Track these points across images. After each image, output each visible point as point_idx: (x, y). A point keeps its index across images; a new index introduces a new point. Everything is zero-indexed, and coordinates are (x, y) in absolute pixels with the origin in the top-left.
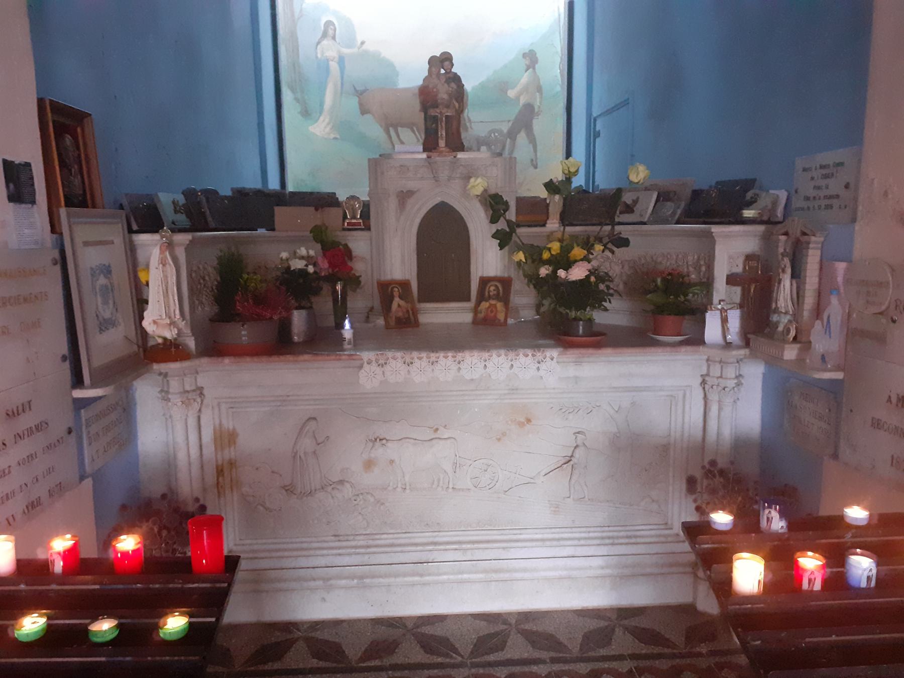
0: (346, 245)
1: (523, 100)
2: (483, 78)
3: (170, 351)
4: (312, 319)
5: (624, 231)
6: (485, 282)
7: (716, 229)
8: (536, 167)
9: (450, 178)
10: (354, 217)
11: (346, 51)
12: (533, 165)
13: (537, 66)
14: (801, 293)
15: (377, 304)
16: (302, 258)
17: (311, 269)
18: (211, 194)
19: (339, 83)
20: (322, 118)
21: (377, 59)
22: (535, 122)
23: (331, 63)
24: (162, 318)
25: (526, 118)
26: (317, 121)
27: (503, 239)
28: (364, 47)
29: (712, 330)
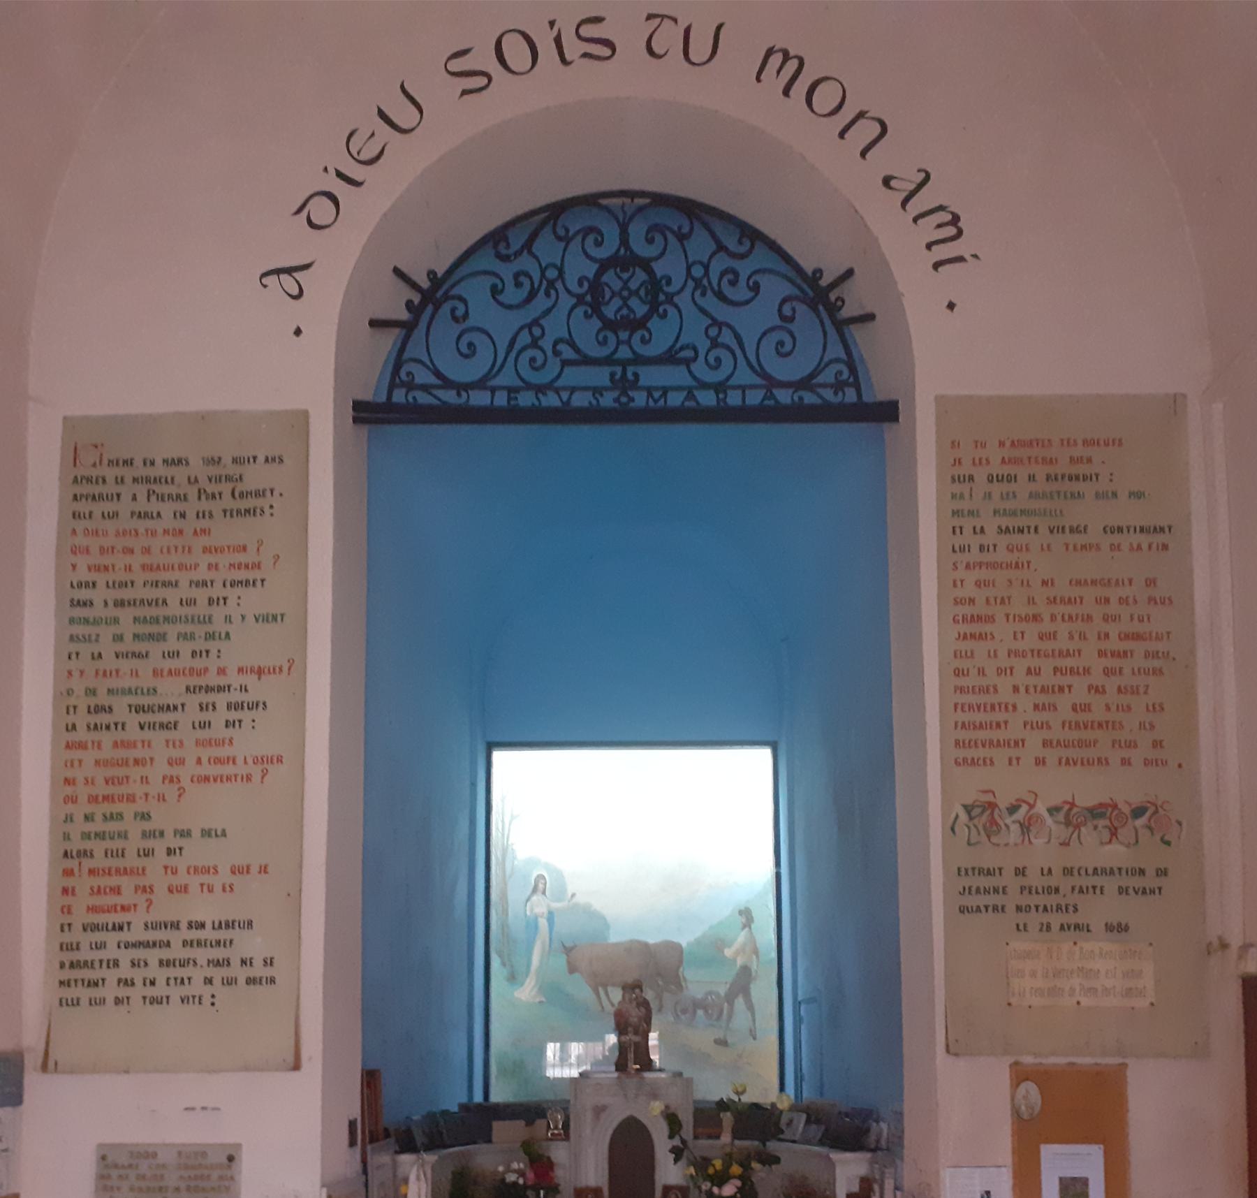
0: (549, 1158)
1: (740, 962)
2: (698, 934)
7: (836, 1156)
8: (755, 1038)
9: (637, 1096)
10: (556, 1128)
16: (515, 1171)
17: (521, 1181)
18: (445, 1113)
22: (752, 986)
25: (743, 982)
26: (522, 985)
27: (678, 1153)
28: (574, 900)
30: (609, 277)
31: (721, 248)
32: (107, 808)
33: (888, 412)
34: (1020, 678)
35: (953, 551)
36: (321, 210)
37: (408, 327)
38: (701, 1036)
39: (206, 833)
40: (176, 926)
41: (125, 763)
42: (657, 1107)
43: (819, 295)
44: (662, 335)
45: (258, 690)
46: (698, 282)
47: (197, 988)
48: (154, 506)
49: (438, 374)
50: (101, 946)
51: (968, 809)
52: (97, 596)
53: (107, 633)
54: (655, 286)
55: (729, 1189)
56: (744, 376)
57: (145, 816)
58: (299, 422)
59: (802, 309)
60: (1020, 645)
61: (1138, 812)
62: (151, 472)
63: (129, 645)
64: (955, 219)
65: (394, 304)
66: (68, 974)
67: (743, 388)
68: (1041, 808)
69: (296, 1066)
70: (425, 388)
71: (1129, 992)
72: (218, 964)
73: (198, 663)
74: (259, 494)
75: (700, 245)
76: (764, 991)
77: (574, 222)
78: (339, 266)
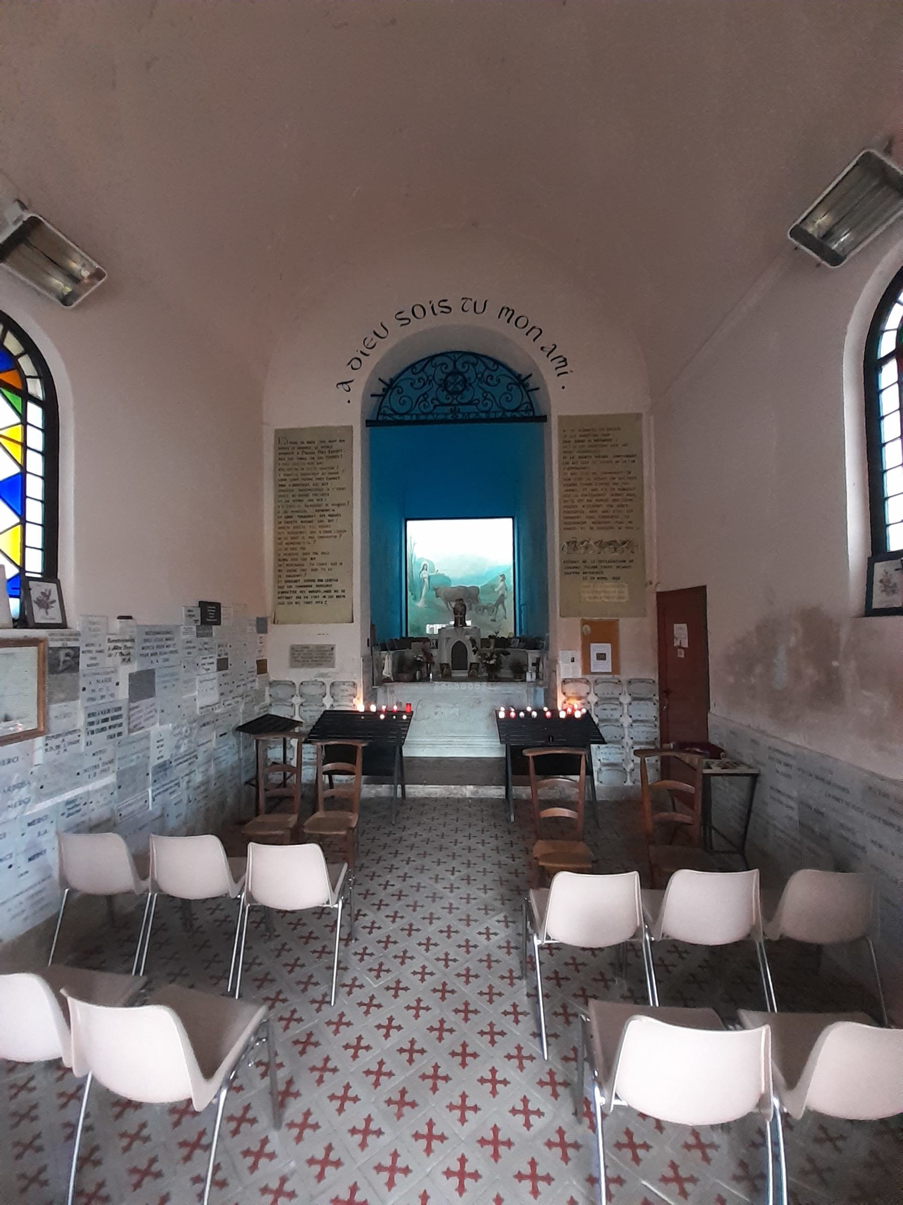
1: (501, 593)
3: (388, 680)
4: (421, 674)
5: (508, 650)
6: (471, 664)
7: (528, 651)
14: (157, 629)
15: (439, 670)
24: (387, 672)
25: (501, 600)
27: (475, 652)
29: (528, 678)
30: (450, 379)
31: (487, 368)
32: (292, 546)
33: (544, 419)
34: (585, 503)
35: (563, 464)
36: (356, 364)
37: (384, 396)
38: (486, 618)
39: (323, 553)
40: (314, 581)
41: (297, 533)
42: (468, 637)
43: (521, 382)
44: (467, 396)
45: (338, 510)
46: (480, 379)
47: (321, 599)
48: (305, 456)
49: (392, 410)
50: (291, 587)
51: (568, 543)
52: (287, 483)
53: (290, 494)
54: (465, 380)
55: (492, 662)
56: (495, 408)
57: (304, 549)
58: (350, 429)
59: (514, 387)
60: (585, 493)
61: (624, 543)
62: (303, 445)
63: (297, 498)
64: (565, 360)
65: (379, 389)
66: (280, 595)
67: (495, 412)
68: (592, 543)
69: (352, 622)
70: (389, 415)
71: (619, 598)
72: (327, 592)
73: (320, 502)
74: (337, 451)
75: (480, 368)
76: (509, 602)
77: (439, 360)
78: (361, 381)
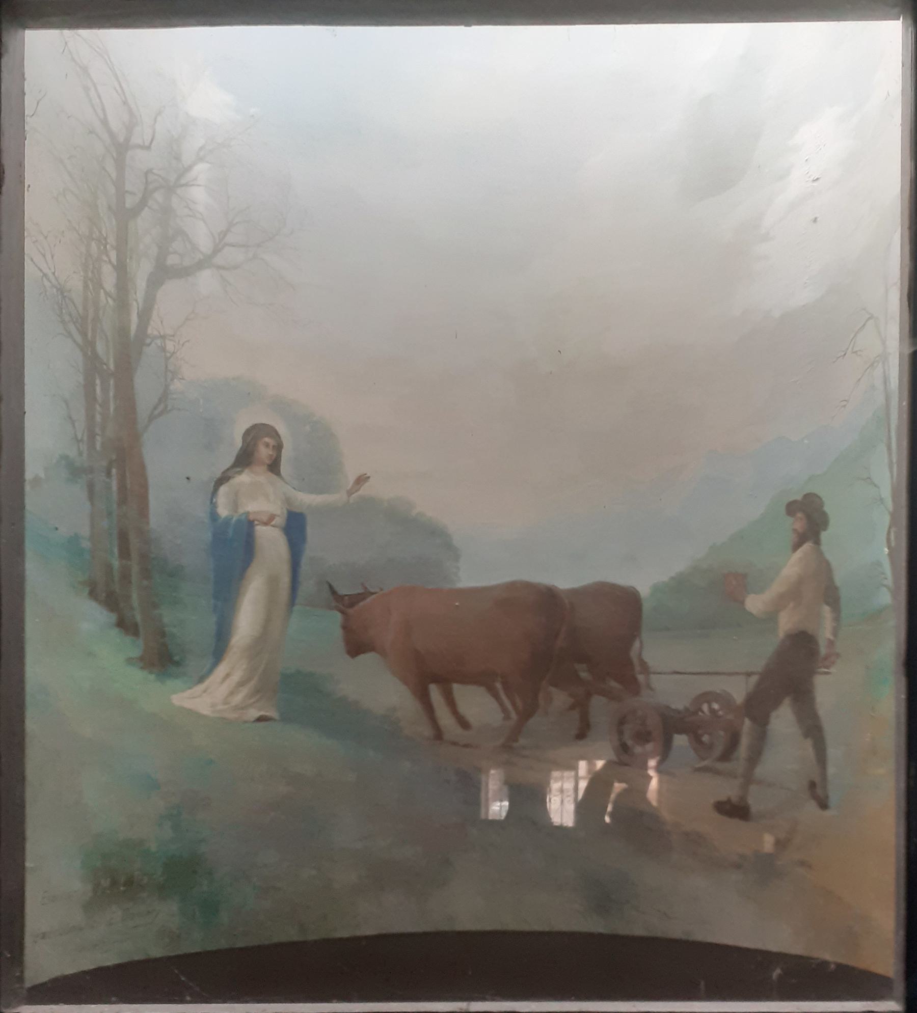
1: (786, 622)
8: (823, 805)
11: (306, 499)
12: (815, 797)
13: (824, 536)
19: (285, 580)
20: (222, 669)
21: (402, 520)
23: (260, 529)
25: (793, 671)
28: (365, 490)
